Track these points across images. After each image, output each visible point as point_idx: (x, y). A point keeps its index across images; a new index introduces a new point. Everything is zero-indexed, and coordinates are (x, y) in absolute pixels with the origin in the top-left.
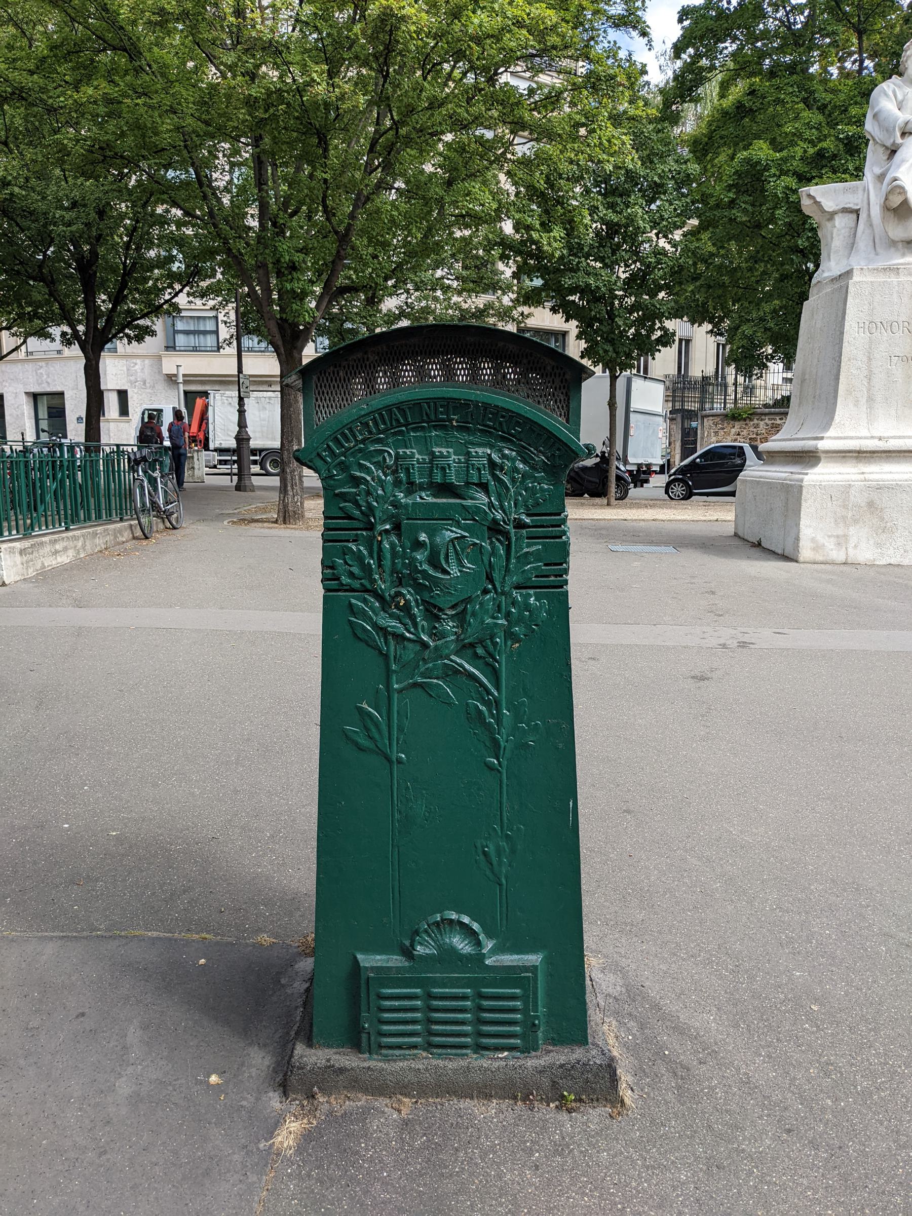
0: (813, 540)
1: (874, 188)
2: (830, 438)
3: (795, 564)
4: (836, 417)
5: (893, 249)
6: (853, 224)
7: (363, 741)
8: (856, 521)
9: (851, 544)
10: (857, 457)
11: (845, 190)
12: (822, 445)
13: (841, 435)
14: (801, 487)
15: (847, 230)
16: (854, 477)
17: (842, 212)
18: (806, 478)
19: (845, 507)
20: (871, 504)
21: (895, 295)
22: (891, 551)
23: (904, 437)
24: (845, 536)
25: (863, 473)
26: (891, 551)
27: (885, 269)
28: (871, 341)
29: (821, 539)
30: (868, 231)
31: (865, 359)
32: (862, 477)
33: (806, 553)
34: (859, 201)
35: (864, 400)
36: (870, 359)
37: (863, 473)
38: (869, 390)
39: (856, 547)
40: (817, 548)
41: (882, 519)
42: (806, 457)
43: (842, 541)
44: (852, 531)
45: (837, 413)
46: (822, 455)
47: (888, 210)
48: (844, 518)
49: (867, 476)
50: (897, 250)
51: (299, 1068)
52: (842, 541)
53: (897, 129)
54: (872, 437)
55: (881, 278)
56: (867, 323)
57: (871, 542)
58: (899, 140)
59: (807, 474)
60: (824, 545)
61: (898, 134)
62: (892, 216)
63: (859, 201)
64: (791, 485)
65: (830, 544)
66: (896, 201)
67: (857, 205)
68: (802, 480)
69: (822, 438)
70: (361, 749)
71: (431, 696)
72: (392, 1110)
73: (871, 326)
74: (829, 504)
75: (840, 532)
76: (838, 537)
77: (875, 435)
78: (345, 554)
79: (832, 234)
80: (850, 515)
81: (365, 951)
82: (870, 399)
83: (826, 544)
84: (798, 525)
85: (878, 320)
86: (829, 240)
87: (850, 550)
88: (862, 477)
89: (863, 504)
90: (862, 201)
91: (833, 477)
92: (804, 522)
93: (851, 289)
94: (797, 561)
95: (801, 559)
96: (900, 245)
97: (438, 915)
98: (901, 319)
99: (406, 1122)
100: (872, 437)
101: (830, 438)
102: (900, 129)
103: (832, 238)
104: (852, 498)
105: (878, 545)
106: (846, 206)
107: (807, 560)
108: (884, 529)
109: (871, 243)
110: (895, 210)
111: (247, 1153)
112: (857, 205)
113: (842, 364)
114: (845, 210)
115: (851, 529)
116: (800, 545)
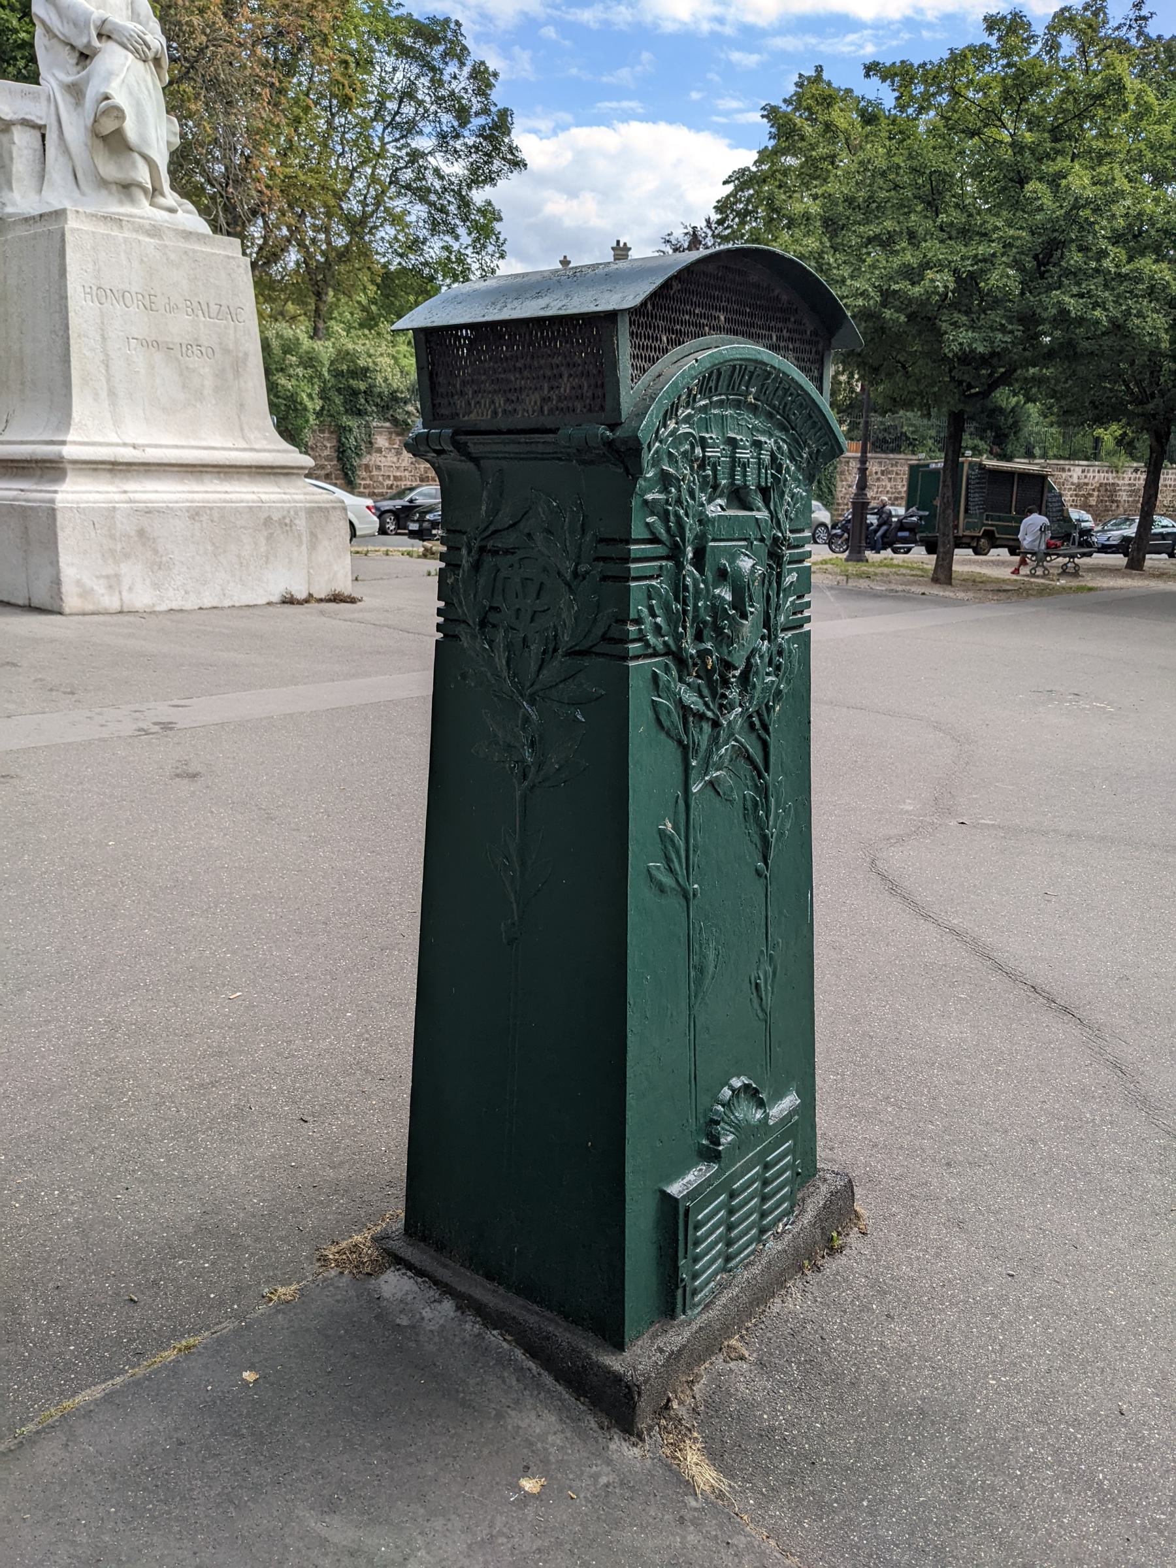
0: (79, 583)
1: (64, 100)
2: (75, 443)
3: (59, 617)
4: (74, 415)
5: (104, 192)
6: (37, 144)
7: (667, 880)
8: (127, 556)
9: (125, 587)
10: (110, 471)
11: (24, 94)
12: (69, 452)
13: (86, 440)
14: (54, 510)
15: (31, 151)
16: (117, 497)
17: (22, 124)
18: (58, 497)
19: (112, 537)
20: (141, 533)
21: (123, 256)
22: (171, 593)
23: (161, 446)
24: (117, 576)
25: (125, 492)
26: (171, 593)
27: (105, 218)
28: (102, 315)
29: (89, 582)
30: (62, 159)
31: (98, 338)
32: (124, 497)
33: (71, 601)
34: (43, 114)
35: (104, 394)
36: (104, 338)
37: (125, 492)
38: (108, 381)
39: (130, 589)
40: (85, 593)
41: (156, 552)
42: (49, 468)
43: (114, 582)
44: (124, 568)
45: (74, 409)
46: (69, 466)
47: (97, 136)
48: (112, 551)
49: (131, 496)
50: (110, 193)
51: (646, 1382)
52: (114, 582)
53: (92, 27)
54: (125, 445)
55: (102, 229)
56: (94, 288)
57: (148, 582)
58: (96, 43)
59: (56, 492)
60: (92, 589)
61: (94, 34)
62: (102, 145)
63: (43, 114)
64: (31, 508)
65: (100, 588)
66: (108, 126)
67: (41, 118)
68: (53, 501)
69: (63, 443)
70: (662, 889)
71: (718, 794)
72: (735, 1362)
73: (101, 293)
74: (93, 534)
75: (109, 571)
76: (108, 577)
77: (127, 441)
78: (650, 598)
79: (10, 153)
80: (119, 547)
81: (671, 1180)
82: (112, 393)
83: (95, 587)
84: (55, 563)
85: (107, 287)
86: (7, 161)
87: (125, 594)
88: (124, 497)
89: (133, 533)
90: (48, 115)
91: (91, 497)
92: (65, 559)
93: (69, 237)
94: (61, 613)
95: (67, 610)
96: (114, 188)
97: (726, 1088)
98: (134, 289)
99: (761, 1364)
100: (125, 445)
101: (75, 443)
102: (97, 28)
103: (11, 159)
104: (119, 525)
105: (156, 586)
106: (28, 117)
107: (74, 610)
108: (159, 566)
109: (71, 177)
110: (104, 139)
111: (696, 1525)
112: (41, 118)
113: (72, 342)
114: (26, 123)
115: (122, 565)
116: (63, 590)
